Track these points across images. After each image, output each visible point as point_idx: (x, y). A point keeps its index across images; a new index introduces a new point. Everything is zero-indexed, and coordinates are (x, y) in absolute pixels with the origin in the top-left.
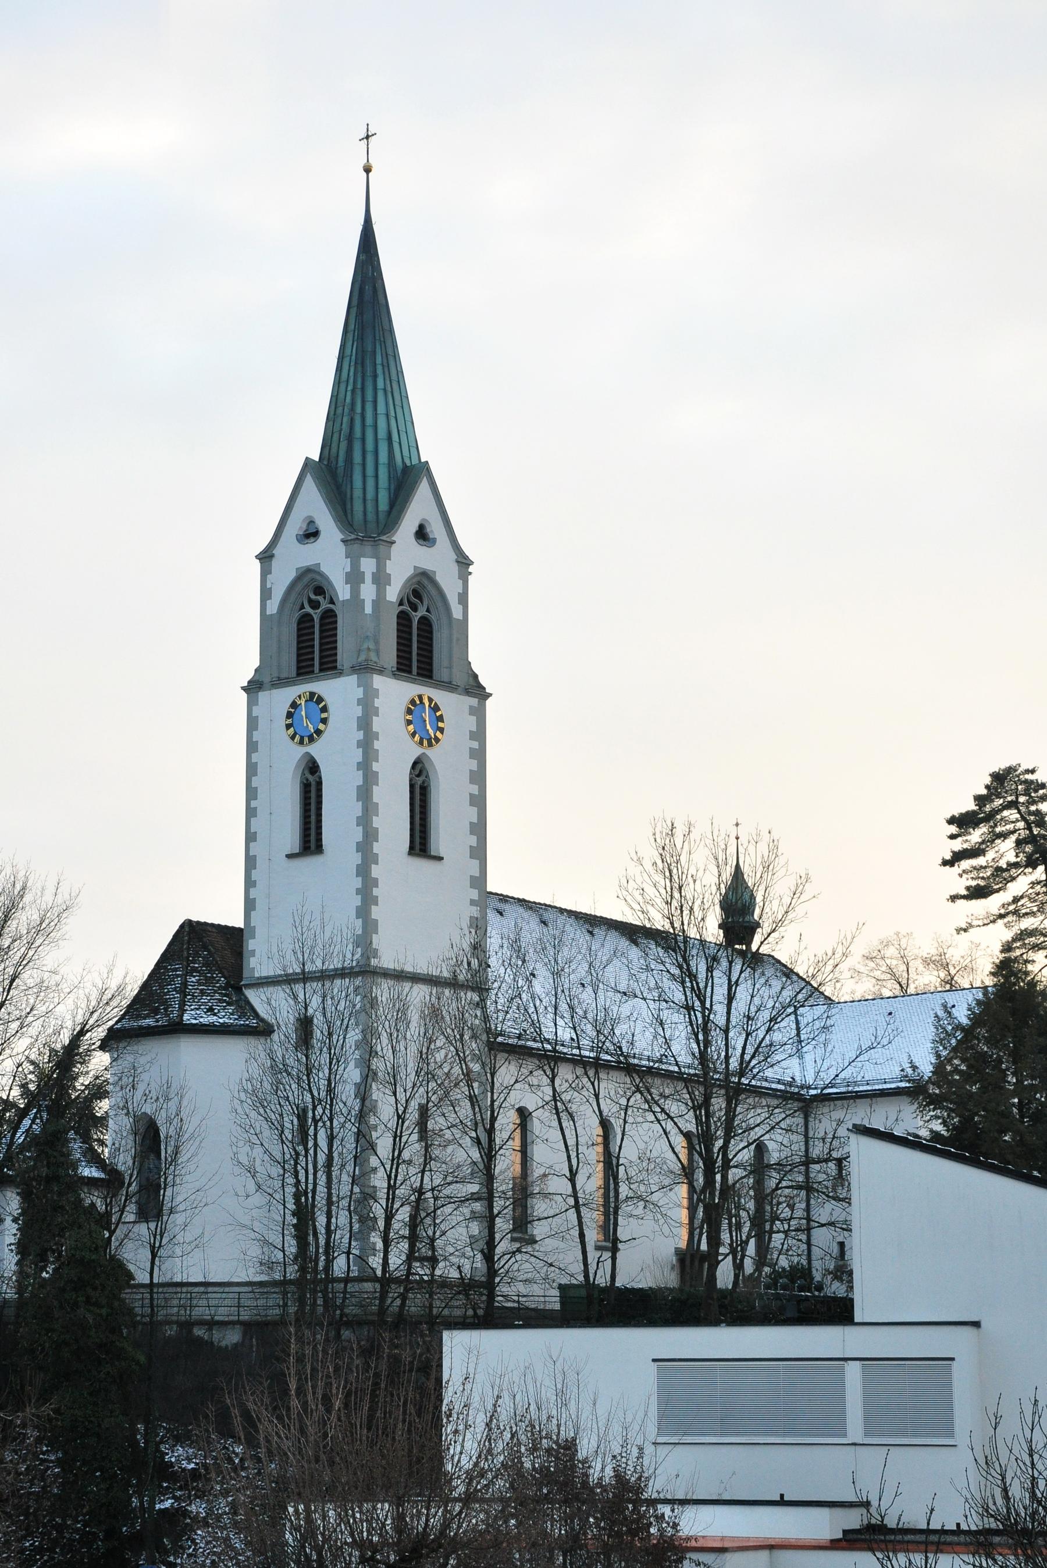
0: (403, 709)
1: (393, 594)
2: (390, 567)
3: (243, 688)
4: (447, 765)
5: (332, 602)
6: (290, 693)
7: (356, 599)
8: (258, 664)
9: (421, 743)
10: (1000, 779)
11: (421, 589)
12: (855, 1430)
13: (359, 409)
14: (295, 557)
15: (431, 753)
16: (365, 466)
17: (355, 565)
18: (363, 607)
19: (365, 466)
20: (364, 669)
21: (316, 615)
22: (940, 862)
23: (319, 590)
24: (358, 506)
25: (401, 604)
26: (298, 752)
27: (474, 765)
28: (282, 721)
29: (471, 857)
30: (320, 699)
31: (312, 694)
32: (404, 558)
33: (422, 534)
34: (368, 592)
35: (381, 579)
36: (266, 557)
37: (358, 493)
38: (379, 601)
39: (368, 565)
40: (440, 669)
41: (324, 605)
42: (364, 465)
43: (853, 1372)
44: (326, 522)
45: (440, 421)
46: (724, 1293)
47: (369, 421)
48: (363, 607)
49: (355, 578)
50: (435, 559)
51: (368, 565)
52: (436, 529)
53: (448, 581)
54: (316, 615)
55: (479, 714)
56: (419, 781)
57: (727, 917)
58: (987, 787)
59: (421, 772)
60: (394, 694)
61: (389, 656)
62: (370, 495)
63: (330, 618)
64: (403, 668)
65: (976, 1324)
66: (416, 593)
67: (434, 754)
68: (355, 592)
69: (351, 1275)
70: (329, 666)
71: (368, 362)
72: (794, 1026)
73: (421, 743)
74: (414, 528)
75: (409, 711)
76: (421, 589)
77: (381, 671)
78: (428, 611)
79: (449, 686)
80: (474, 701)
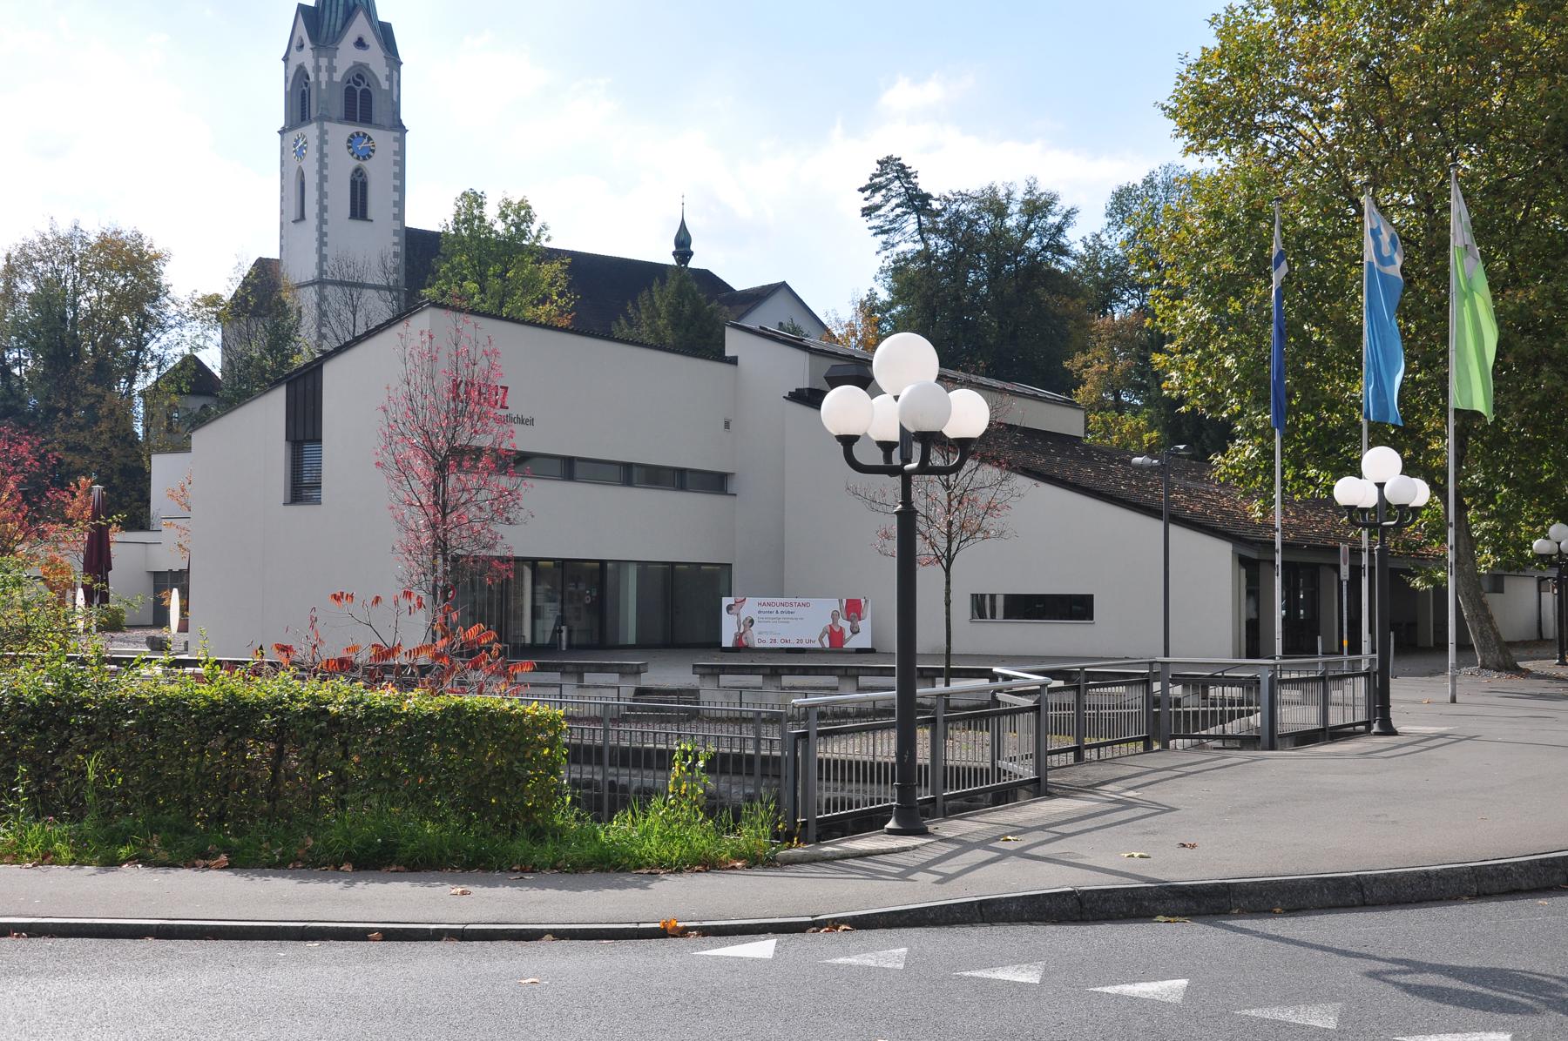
1: (338, 77)
3: (1360, 476)
4: (376, 171)
6: (350, 129)
7: (318, 83)
8: (738, 288)
10: (884, 163)
11: (359, 75)
12: (632, 572)
16: (1172, 809)
17: (317, 62)
18: (683, 246)
19: (1172, 809)
20: (322, 119)
22: (359, 225)
23: (359, 76)
26: (356, 163)
27: (396, 197)
29: (1091, 597)
32: (346, 56)
33: (360, 43)
35: (331, 69)
36: (286, 59)
39: (324, 62)
40: (376, 118)
41: (363, 86)
44: (308, 44)
48: (683, 246)
49: (317, 69)
50: (373, 57)
55: (401, 142)
56: (359, 180)
60: (340, 133)
61: (338, 107)
63: (367, 95)
64: (349, 117)
65: (716, 483)
70: (367, 119)
74: (355, 39)
76: (359, 75)
79: (380, 127)
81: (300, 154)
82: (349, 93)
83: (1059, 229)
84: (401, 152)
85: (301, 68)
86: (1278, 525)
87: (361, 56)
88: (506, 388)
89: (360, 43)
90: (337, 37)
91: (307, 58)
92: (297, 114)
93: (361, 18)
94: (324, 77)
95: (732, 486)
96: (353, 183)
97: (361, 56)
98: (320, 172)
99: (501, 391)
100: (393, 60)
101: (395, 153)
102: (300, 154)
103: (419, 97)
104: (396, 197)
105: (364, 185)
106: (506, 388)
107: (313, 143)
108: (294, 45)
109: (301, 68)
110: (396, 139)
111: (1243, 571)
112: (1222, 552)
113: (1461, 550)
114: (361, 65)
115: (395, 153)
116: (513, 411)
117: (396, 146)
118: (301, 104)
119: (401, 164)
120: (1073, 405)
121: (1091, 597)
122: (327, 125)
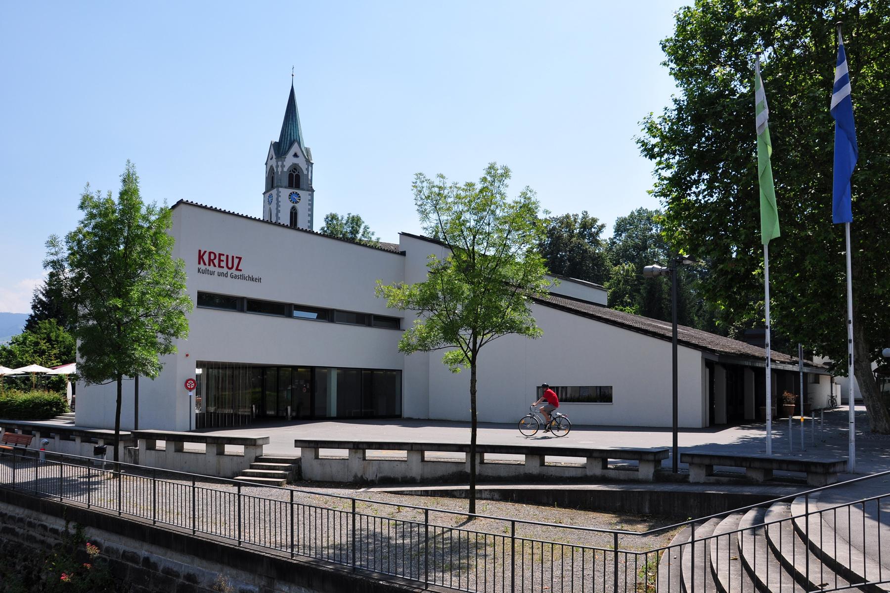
1: (285, 169)
4: (301, 208)
6: (291, 191)
11: (295, 168)
14: (270, 164)
15: (297, 205)
16: (288, 141)
19: (288, 141)
22: (271, 440)
26: (292, 205)
27: (309, 218)
29: (611, 387)
32: (289, 161)
33: (296, 155)
34: (280, 169)
35: (283, 166)
36: (266, 164)
39: (280, 163)
43: (334, 412)
45: (309, 134)
46: (76, 521)
49: (277, 166)
50: (301, 162)
52: (299, 153)
53: (303, 165)
57: (20, 379)
58: (527, 208)
60: (285, 192)
61: (286, 181)
63: (298, 177)
64: (290, 186)
67: (297, 205)
70: (298, 186)
76: (295, 168)
79: (303, 189)
81: (270, 203)
82: (291, 176)
83: (597, 234)
84: (312, 200)
85: (272, 166)
86: (768, 324)
87: (296, 161)
88: (240, 259)
89: (296, 155)
90: (286, 153)
91: (273, 162)
92: (270, 186)
93: (296, 145)
94: (280, 169)
95: (403, 325)
96: (291, 213)
97: (296, 161)
98: (277, 208)
99: (236, 261)
100: (309, 163)
102: (270, 203)
103: (319, 179)
104: (309, 218)
105: (296, 214)
106: (240, 259)
107: (275, 197)
108: (270, 158)
109: (272, 166)
111: (708, 370)
112: (697, 355)
113: (861, 353)
116: (246, 272)
118: (272, 182)
119: (312, 205)
120: (602, 289)
121: (611, 387)
122: (280, 189)
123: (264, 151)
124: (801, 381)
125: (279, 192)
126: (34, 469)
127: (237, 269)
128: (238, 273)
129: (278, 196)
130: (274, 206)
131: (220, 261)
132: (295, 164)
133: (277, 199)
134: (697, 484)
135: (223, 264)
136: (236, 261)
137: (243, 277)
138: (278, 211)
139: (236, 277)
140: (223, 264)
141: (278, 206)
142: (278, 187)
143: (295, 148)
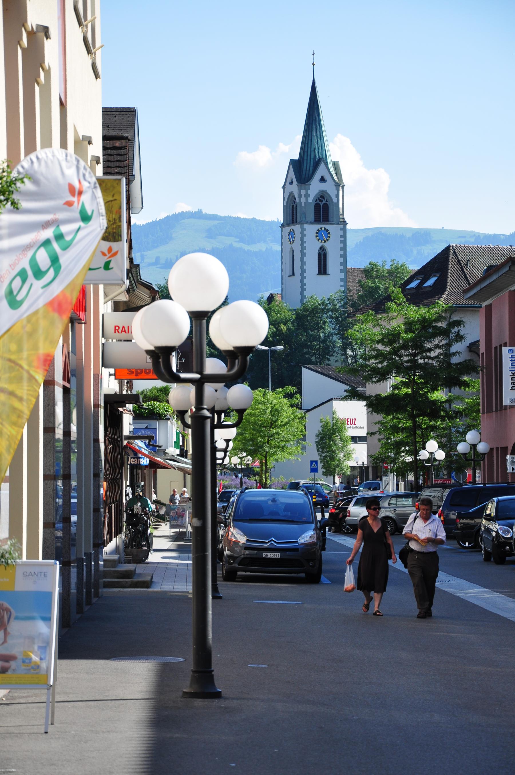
0: (315, 233)
1: (310, 200)
2: (310, 192)
4: (332, 248)
5: (327, 201)
6: (318, 226)
7: (301, 203)
9: (322, 242)
11: (322, 196)
13: (307, 142)
16: (308, 164)
17: (300, 192)
21: (321, 204)
23: (322, 197)
24: (304, 173)
25: (316, 201)
28: (314, 234)
30: (327, 230)
31: (325, 228)
32: (315, 187)
33: (323, 180)
34: (303, 200)
35: (307, 196)
36: (284, 187)
37: (305, 168)
38: (307, 202)
39: (303, 192)
40: (330, 219)
41: (324, 202)
42: (307, 159)
45: (338, 148)
47: (309, 146)
49: (300, 196)
50: (328, 187)
51: (303, 192)
52: (327, 177)
53: (332, 192)
54: (321, 204)
59: (323, 250)
60: (311, 229)
61: (311, 215)
62: (308, 169)
63: (326, 206)
64: (317, 220)
66: (322, 197)
67: (326, 245)
68: (300, 200)
69: (454, 360)
70: (326, 220)
71: (310, 127)
72: (469, 279)
73: (322, 242)
75: (317, 233)
76: (322, 196)
77: (307, 223)
78: (327, 201)
79: (332, 223)
80: (342, 226)
82: (317, 207)
85: (291, 194)
87: (323, 186)
88: (355, 419)
89: (323, 180)
90: (310, 178)
91: (294, 188)
93: (322, 165)
96: (319, 255)
97: (323, 186)
98: (302, 251)
99: (354, 420)
101: (341, 237)
105: (325, 255)
106: (355, 419)
107: (298, 235)
108: (288, 182)
109: (291, 194)
110: (341, 229)
114: (323, 191)
115: (341, 237)
116: (357, 425)
117: (341, 233)
118: (292, 213)
122: (305, 226)
123: (281, 171)
124: (83, 449)
125: (303, 231)
126: (154, 538)
127: (354, 424)
128: (355, 426)
129: (303, 235)
130: (297, 246)
131: (348, 422)
132: (323, 191)
133: (302, 239)
134: (479, 484)
135: (349, 423)
136: (354, 420)
137: (356, 427)
138: (303, 255)
139: (354, 428)
140: (349, 423)
141: (303, 247)
142: (302, 223)
143: (321, 171)
